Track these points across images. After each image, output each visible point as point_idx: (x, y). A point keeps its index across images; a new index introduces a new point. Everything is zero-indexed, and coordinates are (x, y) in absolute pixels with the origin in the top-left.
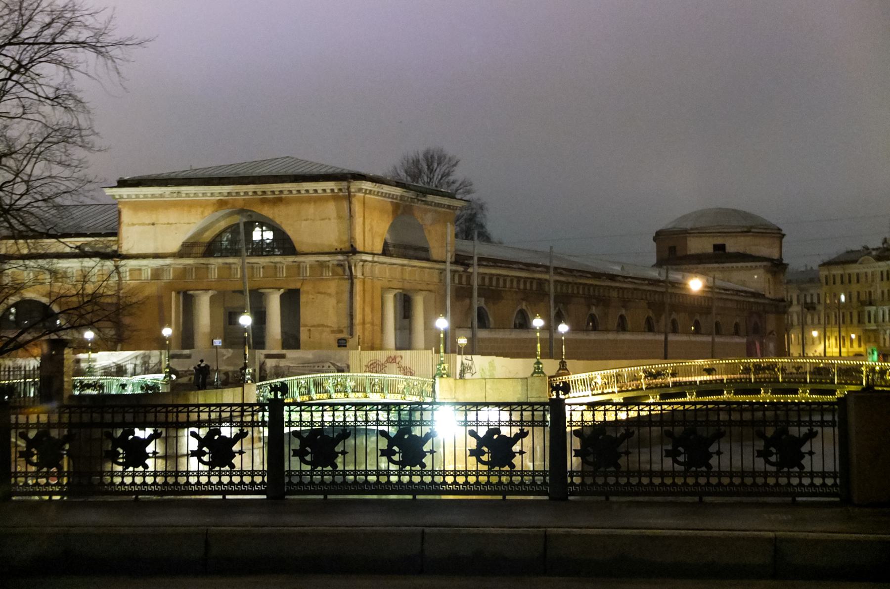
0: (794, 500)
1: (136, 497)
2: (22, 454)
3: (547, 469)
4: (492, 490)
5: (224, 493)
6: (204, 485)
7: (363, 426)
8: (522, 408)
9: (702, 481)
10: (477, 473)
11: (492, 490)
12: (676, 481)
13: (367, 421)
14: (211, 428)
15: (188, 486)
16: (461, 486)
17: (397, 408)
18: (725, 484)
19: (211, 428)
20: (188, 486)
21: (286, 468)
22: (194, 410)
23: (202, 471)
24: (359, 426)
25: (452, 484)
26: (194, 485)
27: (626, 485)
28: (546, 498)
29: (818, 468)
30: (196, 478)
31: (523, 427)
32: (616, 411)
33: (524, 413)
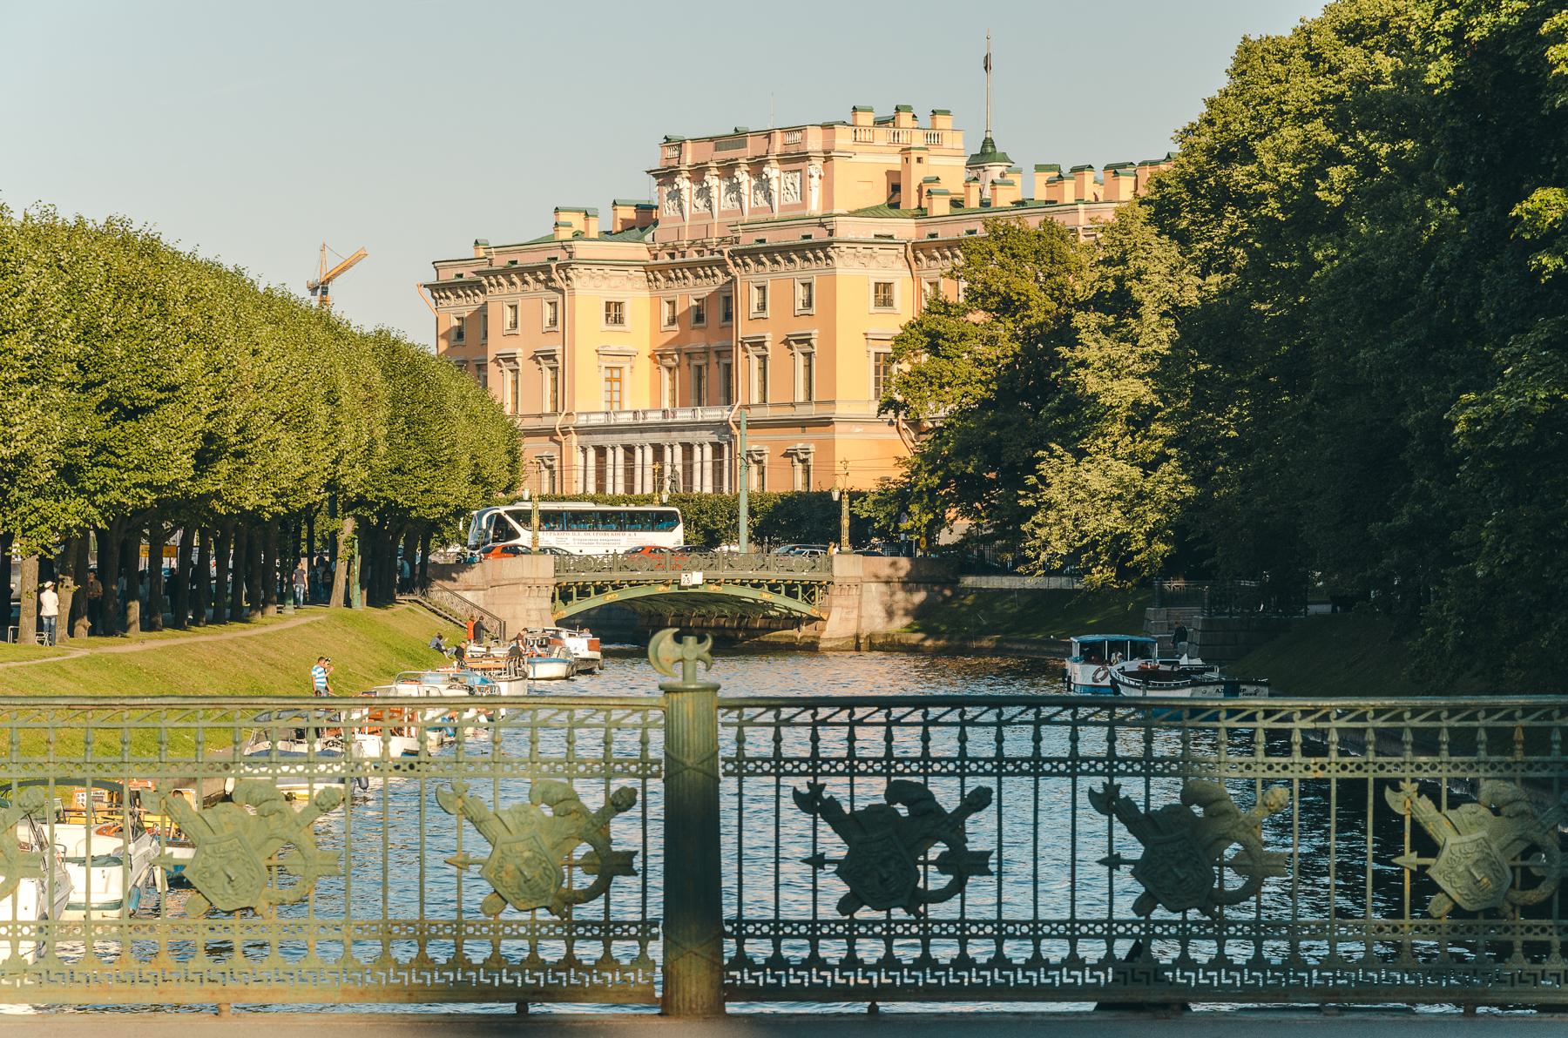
0: (873, 1010)
1: (873, 1010)
2: (623, 863)
3: (656, 911)
4: (424, 984)
5: (524, 996)
6: (1093, 968)
7: (913, 774)
8: (852, 714)
9: (1203, 951)
10: (1000, 929)
11: (424, 984)
12: (1228, 951)
13: (570, 759)
14: (893, 779)
15: (567, 970)
16: (1315, 974)
17: (1030, 716)
18: (942, 961)
19: (893, 779)
20: (567, 970)
21: (729, 911)
22: (798, 719)
23: (1084, 923)
24: (902, 774)
25: (989, 966)
26: (1058, 967)
27: (806, 965)
28: (1090, 1006)
29: (1018, 907)
30: (1029, 946)
31: (1116, 781)
32: (852, 724)
33: (860, 732)
